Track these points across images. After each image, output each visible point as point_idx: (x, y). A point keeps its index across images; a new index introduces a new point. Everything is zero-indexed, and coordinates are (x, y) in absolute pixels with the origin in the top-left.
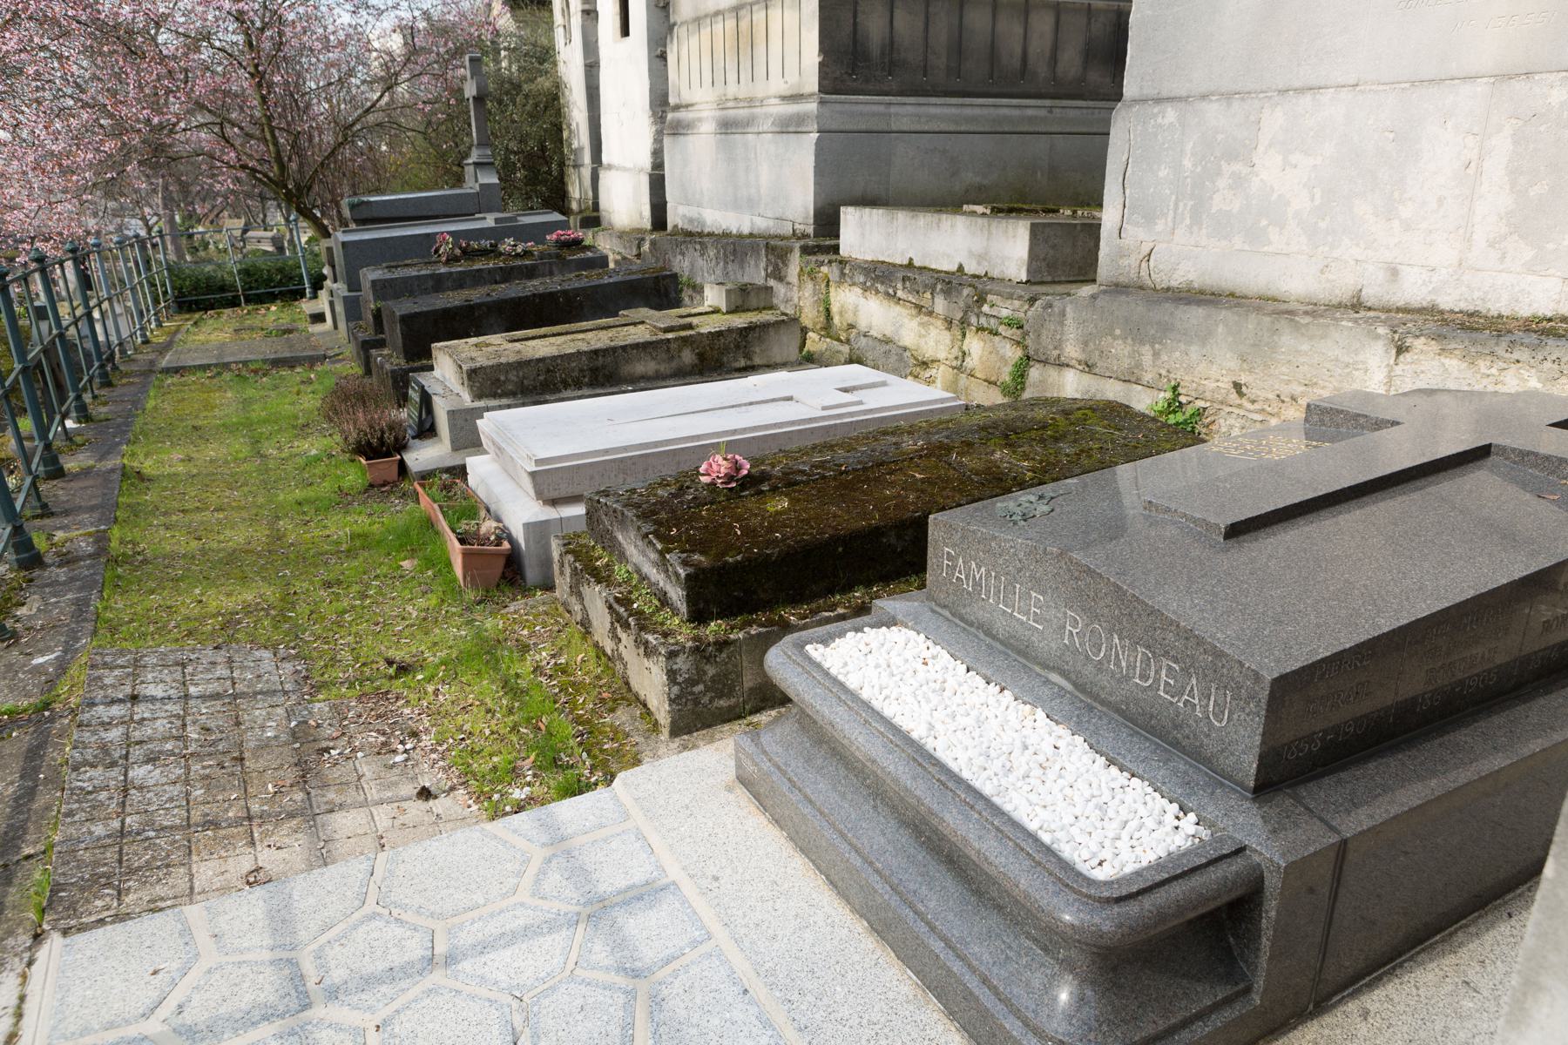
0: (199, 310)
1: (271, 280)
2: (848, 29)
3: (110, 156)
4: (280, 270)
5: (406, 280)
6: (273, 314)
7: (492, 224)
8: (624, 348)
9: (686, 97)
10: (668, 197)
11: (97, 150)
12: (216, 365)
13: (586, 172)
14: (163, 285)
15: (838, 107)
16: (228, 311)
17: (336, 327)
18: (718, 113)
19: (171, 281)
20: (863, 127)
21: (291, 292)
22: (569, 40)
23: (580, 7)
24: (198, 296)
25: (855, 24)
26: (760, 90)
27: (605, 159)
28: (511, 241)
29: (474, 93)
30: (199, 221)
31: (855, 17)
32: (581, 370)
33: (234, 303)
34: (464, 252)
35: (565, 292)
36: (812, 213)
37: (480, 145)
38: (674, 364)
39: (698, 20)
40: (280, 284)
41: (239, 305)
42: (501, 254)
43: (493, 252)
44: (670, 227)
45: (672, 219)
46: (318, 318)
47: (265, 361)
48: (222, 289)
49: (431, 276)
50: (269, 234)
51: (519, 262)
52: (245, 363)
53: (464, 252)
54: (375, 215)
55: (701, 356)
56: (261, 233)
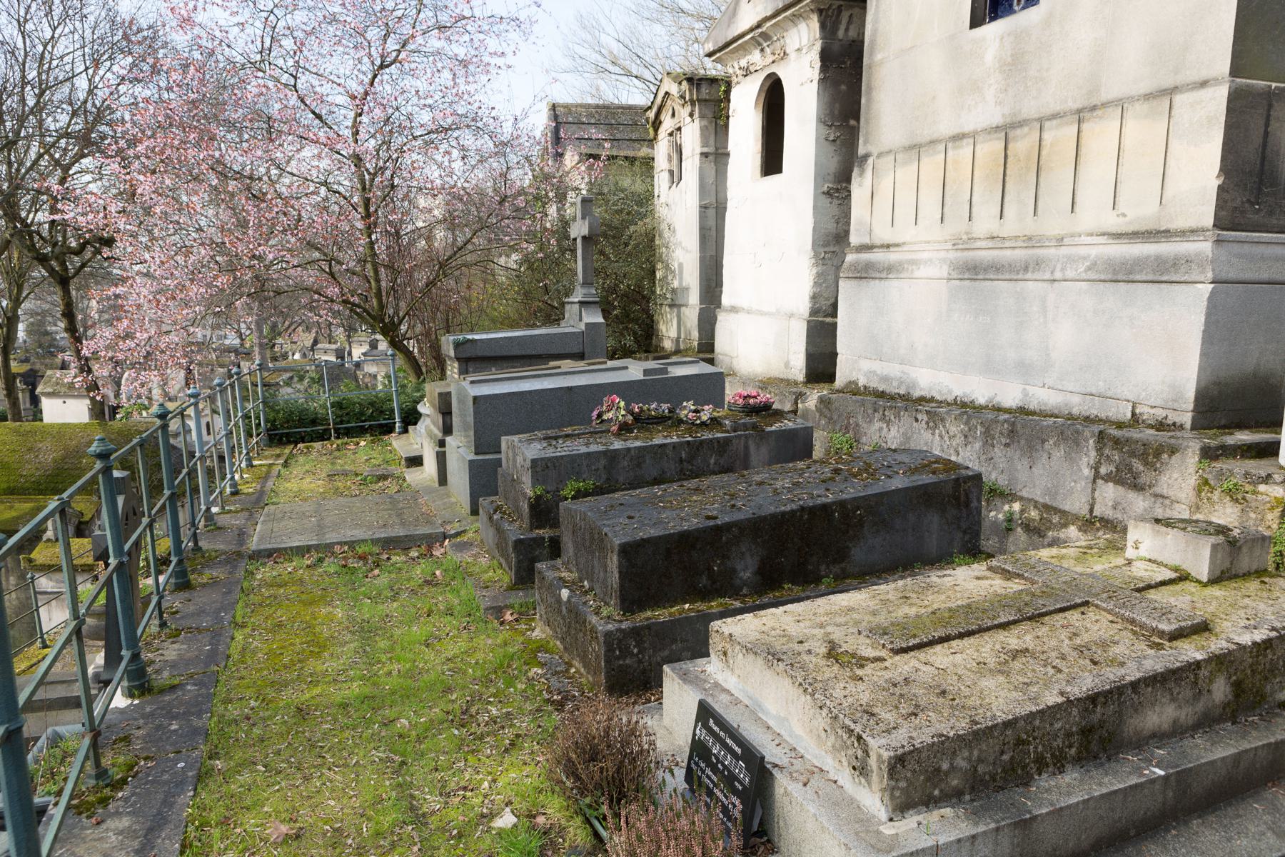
0: (289, 442)
1: (362, 414)
2: (1257, 140)
3: (223, 290)
4: (372, 404)
5: (573, 459)
6: (362, 453)
7: (640, 376)
8: (1134, 685)
9: (883, 234)
10: (840, 348)
11: (209, 285)
12: (317, 548)
13: (691, 314)
14: (258, 417)
15: (1236, 248)
16: (317, 445)
17: (443, 479)
18: (952, 255)
19: (265, 412)
20: (1265, 276)
21: (381, 426)
22: (675, 177)
23: (698, 150)
24: (289, 430)
25: (1266, 134)
26: (1052, 224)
27: (726, 300)
28: (690, 405)
29: (585, 231)
30: (279, 334)
31: (1267, 125)
32: (1069, 735)
33: (323, 437)
34: (637, 418)
35: (842, 504)
36: (1191, 394)
37: (586, 283)
38: (1200, 707)
39: (916, 149)
40: (371, 418)
41: (329, 439)
42: (681, 421)
43: (670, 421)
44: (840, 380)
45: (843, 373)
46: (416, 461)
47: (375, 542)
48: (314, 422)
49: (605, 453)
50: (334, 347)
51: (707, 435)
52: (352, 544)
53: (637, 418)
54: (480, 354)
55: (1238, 687)
56: (327, 346)
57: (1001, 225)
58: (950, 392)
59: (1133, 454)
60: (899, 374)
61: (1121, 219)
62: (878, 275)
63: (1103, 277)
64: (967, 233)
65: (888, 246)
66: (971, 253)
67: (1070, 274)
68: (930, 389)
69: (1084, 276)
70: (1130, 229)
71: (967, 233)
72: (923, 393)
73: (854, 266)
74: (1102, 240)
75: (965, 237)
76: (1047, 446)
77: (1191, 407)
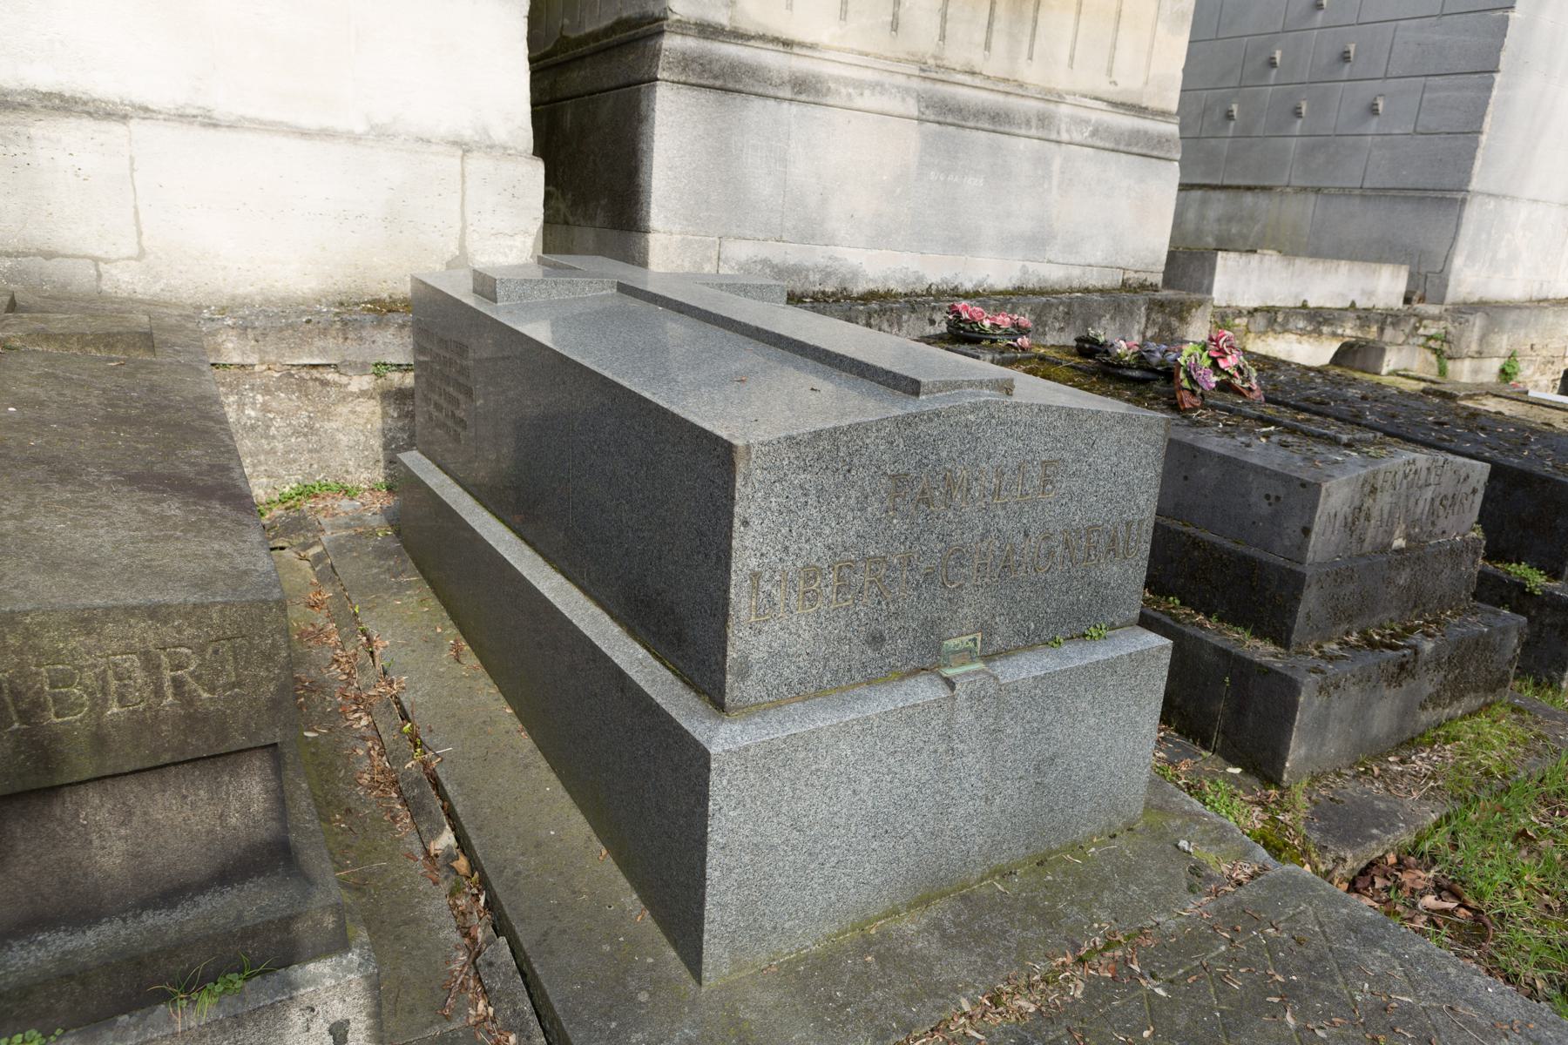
57: (986, 59)
58: (920, 279)
59: (1172, 314)
60: (822, 262)
61: (1112, 87)
62: (771, 91)
63: (1107, 145)
64: (936, 58)
65: (787, 44)
66: (939, 86)
67: (1077, 137)
68: (886, 279)
69: (1090, 141)
70: (1119, 99)
71: (936, 58)
72: (872, 286)
73: (685, 61)
74: (1103, 106)
75: (931, 62)
76: (1103, 322)
77: (1163, 268)
